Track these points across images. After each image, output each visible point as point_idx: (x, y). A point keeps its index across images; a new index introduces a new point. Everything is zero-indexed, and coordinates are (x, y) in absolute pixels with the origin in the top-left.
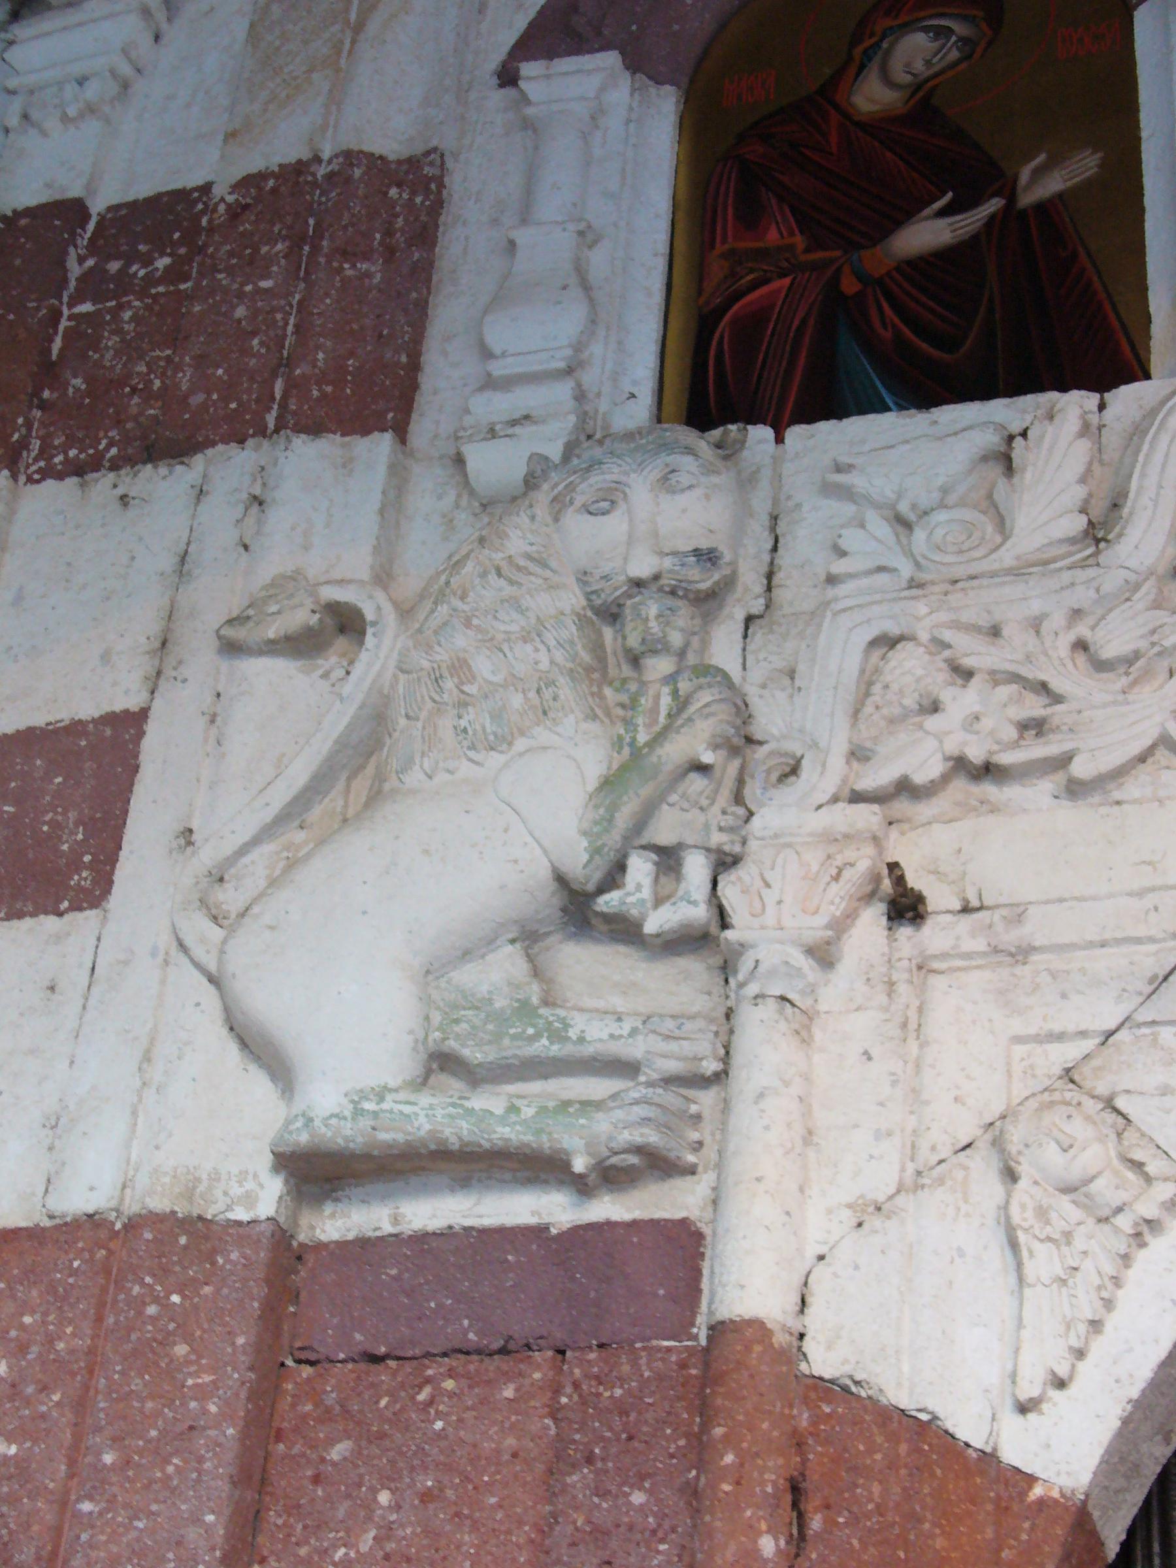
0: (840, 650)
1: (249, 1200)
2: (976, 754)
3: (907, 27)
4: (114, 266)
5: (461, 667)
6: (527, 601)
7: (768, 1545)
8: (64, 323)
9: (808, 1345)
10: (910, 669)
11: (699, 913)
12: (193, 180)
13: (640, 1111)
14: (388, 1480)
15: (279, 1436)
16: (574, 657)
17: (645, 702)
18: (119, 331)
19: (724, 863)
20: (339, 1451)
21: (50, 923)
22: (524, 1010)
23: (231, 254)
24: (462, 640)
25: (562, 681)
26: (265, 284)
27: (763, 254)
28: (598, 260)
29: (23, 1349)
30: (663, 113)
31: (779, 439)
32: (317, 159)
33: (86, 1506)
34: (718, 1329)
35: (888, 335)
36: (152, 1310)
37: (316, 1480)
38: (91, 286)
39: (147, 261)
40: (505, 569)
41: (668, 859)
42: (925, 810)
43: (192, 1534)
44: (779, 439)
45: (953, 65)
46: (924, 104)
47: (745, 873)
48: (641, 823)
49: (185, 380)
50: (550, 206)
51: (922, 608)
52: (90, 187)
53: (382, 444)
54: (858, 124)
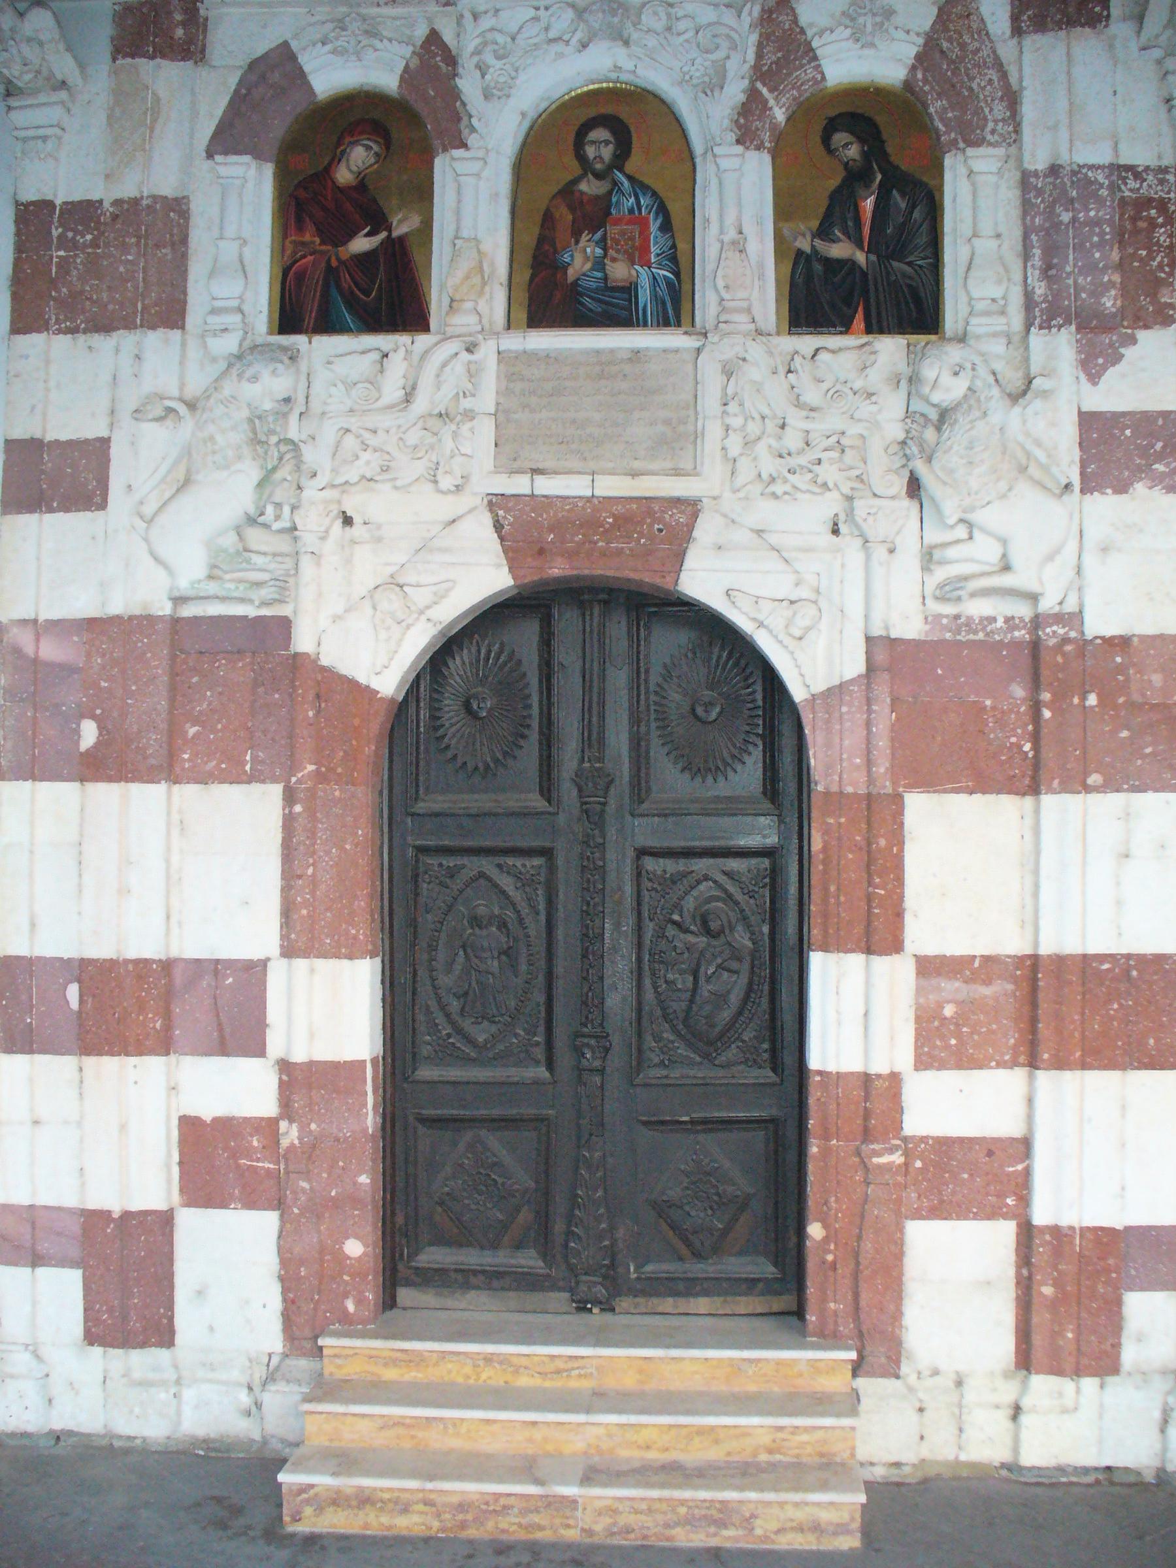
0: (328, 433)
1: (162, 609)
2: (368, 476)
3: (356, 143)
4: (70, 234)
5: (212, 438)
7: (311, 714)
8: (55, 260)
11: (288, 525)
12: (95, 196)
13: (273, 589)
14: (210, 689)
15: (177, 675)
17: (270, 453)
19: (294, 508)
20: (195, 680)
21: (88, 513)
22: (238, 553)
23: (115, 239)
24: (211, 428)
27: (303, 244)
28: (247, 252)
30: (269, 170)
31: (310, 342)
32: (142, 198)
34: (296, 655)
38: (63, 242)
39: (83, 236)
41: (278, 506)
42: (353, 489)
44: (310, 342)
45: (371, 165)
46: (361, 186)
47: (301, 511)
48: (270, 496)
49: (105, 295)
50: (231, 231)
51: (353, 420)
52: (55, 196)
53: (176, 334)
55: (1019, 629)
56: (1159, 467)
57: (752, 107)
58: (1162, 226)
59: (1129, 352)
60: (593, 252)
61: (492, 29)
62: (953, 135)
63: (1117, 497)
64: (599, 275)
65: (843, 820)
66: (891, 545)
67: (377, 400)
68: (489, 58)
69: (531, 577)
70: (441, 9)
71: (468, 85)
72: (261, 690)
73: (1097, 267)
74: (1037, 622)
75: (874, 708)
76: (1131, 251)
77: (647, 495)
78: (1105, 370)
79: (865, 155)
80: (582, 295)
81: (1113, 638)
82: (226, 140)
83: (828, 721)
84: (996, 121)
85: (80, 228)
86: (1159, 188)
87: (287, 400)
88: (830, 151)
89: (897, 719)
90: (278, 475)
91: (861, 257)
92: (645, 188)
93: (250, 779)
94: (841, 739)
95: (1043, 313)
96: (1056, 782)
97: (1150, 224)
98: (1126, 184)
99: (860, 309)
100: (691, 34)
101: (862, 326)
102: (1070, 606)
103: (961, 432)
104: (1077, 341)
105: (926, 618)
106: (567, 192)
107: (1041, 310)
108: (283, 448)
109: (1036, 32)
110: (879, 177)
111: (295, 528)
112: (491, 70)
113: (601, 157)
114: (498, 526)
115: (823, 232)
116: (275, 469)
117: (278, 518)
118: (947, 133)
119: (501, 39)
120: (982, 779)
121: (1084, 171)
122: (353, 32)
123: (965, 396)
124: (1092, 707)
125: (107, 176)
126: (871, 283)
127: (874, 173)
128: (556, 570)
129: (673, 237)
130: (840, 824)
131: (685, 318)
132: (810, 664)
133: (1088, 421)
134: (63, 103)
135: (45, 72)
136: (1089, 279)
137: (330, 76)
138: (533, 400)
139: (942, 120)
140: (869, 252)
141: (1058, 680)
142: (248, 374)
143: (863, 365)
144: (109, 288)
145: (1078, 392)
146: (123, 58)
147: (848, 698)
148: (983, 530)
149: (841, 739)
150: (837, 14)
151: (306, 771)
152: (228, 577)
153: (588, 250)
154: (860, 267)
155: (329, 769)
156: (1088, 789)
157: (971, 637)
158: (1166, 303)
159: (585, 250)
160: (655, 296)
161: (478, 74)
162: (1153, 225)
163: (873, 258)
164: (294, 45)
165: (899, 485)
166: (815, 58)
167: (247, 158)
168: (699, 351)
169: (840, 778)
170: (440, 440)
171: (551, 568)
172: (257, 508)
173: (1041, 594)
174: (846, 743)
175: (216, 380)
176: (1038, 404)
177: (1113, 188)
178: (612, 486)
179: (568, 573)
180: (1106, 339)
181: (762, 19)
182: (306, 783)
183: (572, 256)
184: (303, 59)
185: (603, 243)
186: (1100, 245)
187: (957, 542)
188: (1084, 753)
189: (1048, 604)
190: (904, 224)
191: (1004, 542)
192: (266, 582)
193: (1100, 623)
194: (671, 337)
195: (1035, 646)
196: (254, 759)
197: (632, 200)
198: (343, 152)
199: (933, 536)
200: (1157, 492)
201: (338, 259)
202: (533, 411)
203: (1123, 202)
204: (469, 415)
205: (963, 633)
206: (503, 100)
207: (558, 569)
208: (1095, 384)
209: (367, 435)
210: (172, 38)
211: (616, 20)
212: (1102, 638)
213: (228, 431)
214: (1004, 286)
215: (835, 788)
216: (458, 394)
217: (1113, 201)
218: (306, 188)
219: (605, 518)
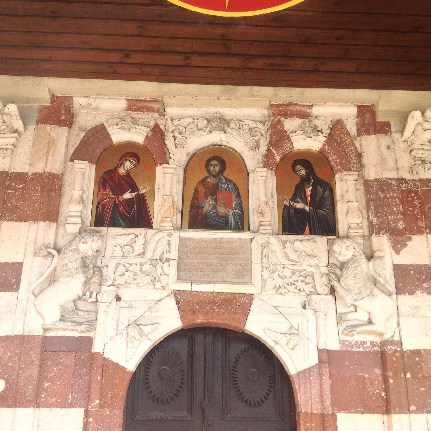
3: (127, 160)
4: (14, 184)
5: (66, 264)
6: (75, 256)
7: (99, 378)
9: (104, 354)
10: (121, 269)
12: (25, 171)
13: (87, 326)
16: (81, 264)
18: (15, 197)
23: (32, 187)
24: (66, 261)
25: (80, 268)
26: (37, 194)
28: (85, 196)
29: (11, 352)
33: (21, 372)
34: (94, 353)
35: (121, 211)
36: (27, 348)
37: (47, 366)
40: (73, 251)
42: (122, 286)
43: (33, 374)
46: (128, 175)
49: (26, 208)
54: (120, 176)
55: (376, 347)
56: (425, 285)
57: (268, 155)
58: (417, 199)
59: (409, 243)
60: (213, 203)
61: (178, 125)
62: (339, 167)
63: (410, 296)
64: (214, 211)
65: (313, 425)
66: (326, 313)
67: (133, 253)
68: (177, 134)
69: (190, 323)
70: (160, 117)
71: (169, 143)
72: (78, 368)
73: (395, 212)
74: (383, 344)
75: (324, 378)
76: (406, 208)
77: (234, 292)
78: (401, 249)
79: (307, 173)
80: (208, 218)
81: (414, 350)
82: (78, 155)
83: (305, 383)
84: (354, 163)
85: (18, 182)
86: (414, 187)
87: (98, 251)
88: (295, 172)
89: (332, 382)
90: (93, 280)
91: (307, 208)
92: (231, 181)
93: (71, 406)
94: (311, 391)
95: (374, 229)
96: (397, 409)
97: (412, 199)
98: (402, 185)
99: (308, 226)
100: (248, 130)
101: (308, 232)
102: (396, 338)
103: (351, 271)
104: (390, 239)
105: (340, 342)
106: (204, 181)
107: (376, 228)
108: (95, 269)
109: (366, 135)
110: (313, 181)
111: (97, 301)
112: (178, 138)
113: (215, 170)
114: (178, 302)
115: (294, 199)
116: (91, 278)
117: (90, 297)
118: (337, 166)
119: (181, 128)
120: (367, 408)
121: (387, 180)
122: (128, 122)
123: (352, 258)
124: (408, 378)
125: (30, 164)
126: (311, 217)
127: (311, 180)
128: (199, 320)
129: (241, 199)
130: (312, 426)
131: (246, 227)
132: (296, 359)
133: (397, 268)
134: (16, 137)
135: (10, 126)
136: (392, 217)
137: (118, 136)
138: (191, 255)
139: (334, 162)
140: (310, 206)
141: (394, 367)
142: (83, 240)
143: (313, 246)
144: (28, 205)
145: (392, 257)
146: (41, 124)
147: (312, 373)
148: (360, 308)
149: (311, 391)
150: (298, 127)
151: (95, 403)
152: (67, 320)
153: (211, 202)
154: (307, 212)
155: (105, 402)
156: (410, 412)
157: (358, 350)
158: (421, 226)
159: (209, 203)
160: (234, 219)
161: (173, 139)
162: (413, 199)
163: (311, 208)
164: (106, 125)
165: (327, 290)
166: (290, 140)
167: (86, 162)
168: (252, 239)
169: (311, 406)
170: (156, 269)
171: (197, 319)
172: (83, 293)
173: (385, 333)
174: (313, 392)
175: (70, 242)
176: (377, 261)
177: (398, 186)
178: (221, 288)
179: (204, 321)
180: (400, 238)
181: (271, 127)
182: (95, 408)
183: (205, 204)
184: (108, 130)
185: (216, 200)
186: (396, 206)
187: (351, 312)
188: (408, 397)
189: (387, 336)
190: (322, 197)
191: (369, 313)
192: (83, 323)
193: (408, 345)
194: (242, 234)
195: (383, 354)
196: (73, 398)
197: (226, 185)
198: (122, 163)
199: (340, 310)
200: (425, 295)
201: (118, 200)
202: (191, 259)
203: (402, 191)
204: (168, 260)
205: (355, 348)
206: (182, 148)
207: (200, 320)
208: (398, 254)
209: (127, 265)
210: (60, 119)
211: (221, 124)
212: (410, 351)
213: (72, 261)
214: (361, 219)
215: (309, 411)
216: (164, 252)
217: (398, 191)
218: (107, 175)
219: (218, 300)
